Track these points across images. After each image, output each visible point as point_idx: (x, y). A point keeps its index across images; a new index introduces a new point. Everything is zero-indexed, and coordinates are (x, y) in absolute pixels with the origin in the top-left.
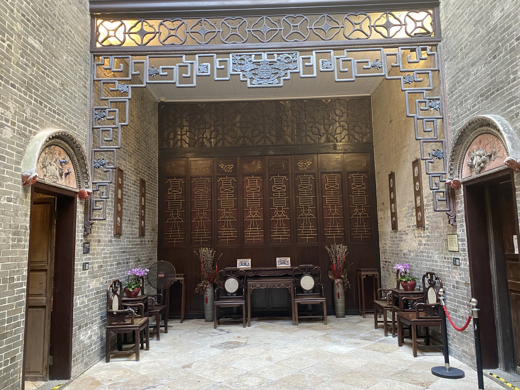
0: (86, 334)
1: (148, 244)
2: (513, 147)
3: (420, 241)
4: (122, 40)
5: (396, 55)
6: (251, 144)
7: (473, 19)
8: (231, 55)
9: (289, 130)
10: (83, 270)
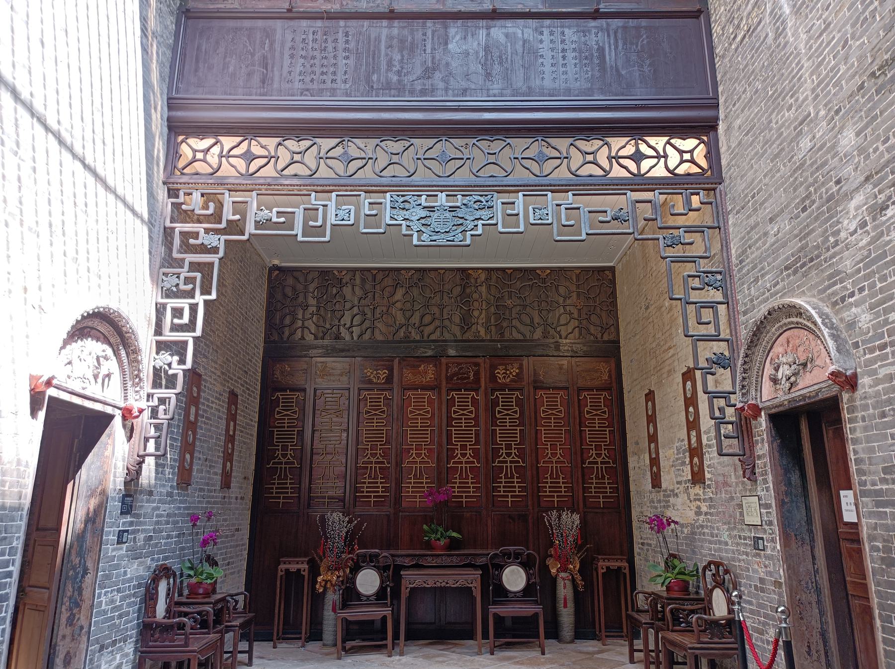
0: (111, 661)
1: (236, 504)
2: (838, 350)
3: (699, 507)
4: (215, 166)
5: (650, 202)
6: (418, 338)
7: (769, 151)
8: (388, 195)
9: (483, 316)
10: (118, 543)
